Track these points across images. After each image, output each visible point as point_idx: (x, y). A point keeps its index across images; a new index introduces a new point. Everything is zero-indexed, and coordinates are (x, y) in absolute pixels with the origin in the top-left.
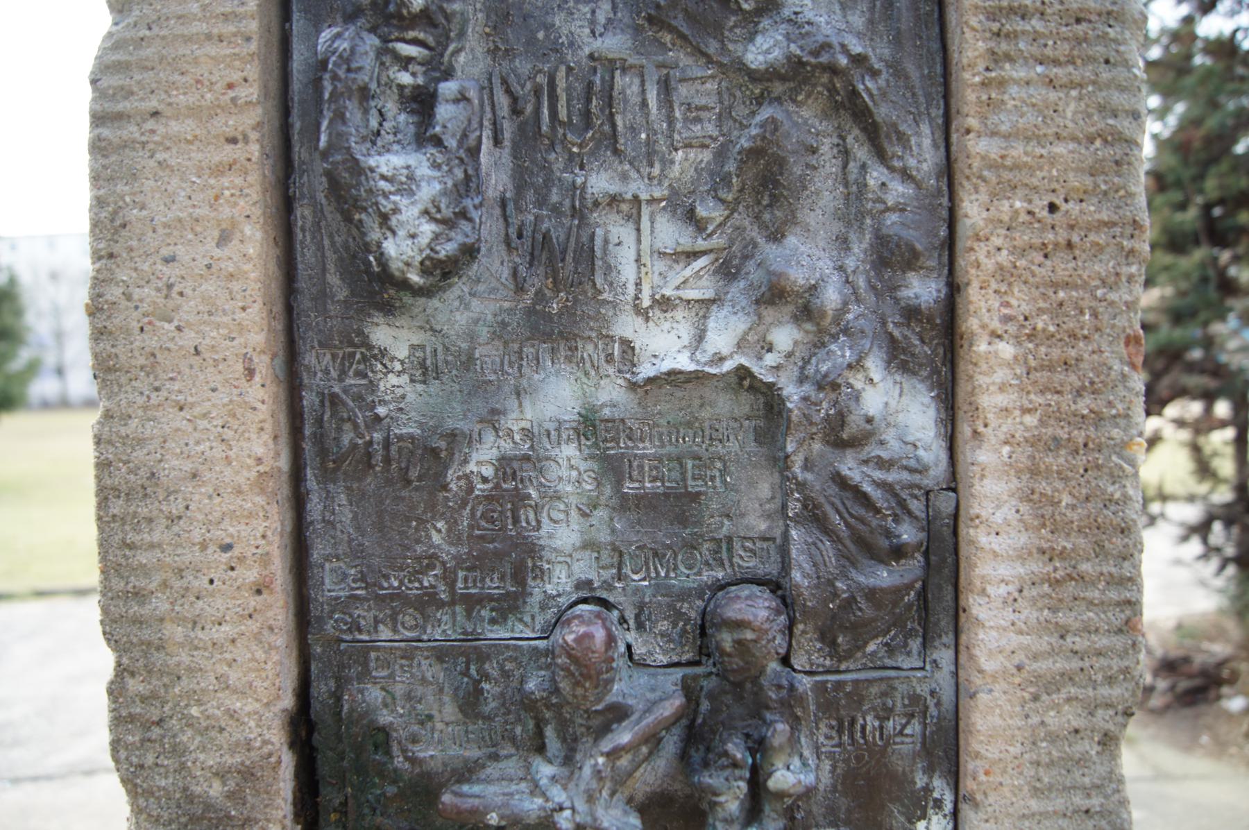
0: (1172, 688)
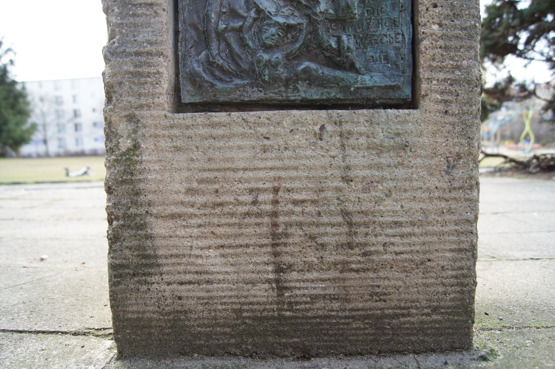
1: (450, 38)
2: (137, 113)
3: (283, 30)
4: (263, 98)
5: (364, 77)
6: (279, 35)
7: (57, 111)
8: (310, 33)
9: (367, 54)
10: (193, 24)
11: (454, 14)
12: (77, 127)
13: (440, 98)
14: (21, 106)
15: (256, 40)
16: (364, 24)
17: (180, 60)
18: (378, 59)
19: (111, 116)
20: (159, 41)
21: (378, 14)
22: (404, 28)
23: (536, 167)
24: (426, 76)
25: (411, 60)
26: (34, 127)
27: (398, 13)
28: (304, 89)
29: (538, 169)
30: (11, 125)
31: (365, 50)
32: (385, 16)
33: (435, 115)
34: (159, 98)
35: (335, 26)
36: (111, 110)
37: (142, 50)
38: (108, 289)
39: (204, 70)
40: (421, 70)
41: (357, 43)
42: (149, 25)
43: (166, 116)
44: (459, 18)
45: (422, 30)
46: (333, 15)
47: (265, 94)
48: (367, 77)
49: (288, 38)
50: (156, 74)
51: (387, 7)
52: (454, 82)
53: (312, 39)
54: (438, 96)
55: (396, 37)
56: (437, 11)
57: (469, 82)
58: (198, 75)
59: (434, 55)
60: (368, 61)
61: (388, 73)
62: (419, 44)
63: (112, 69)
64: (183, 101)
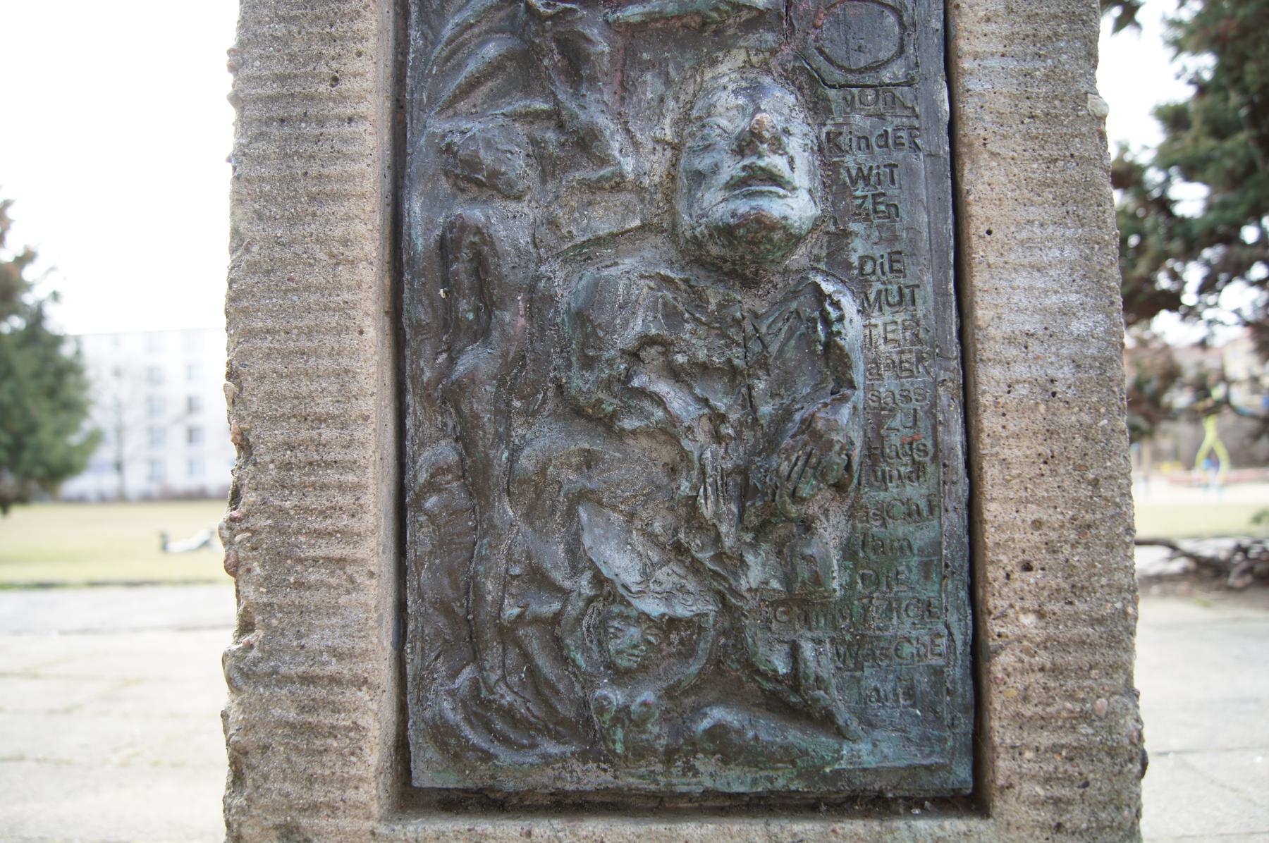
1: (1064, 647)
2: (304, 822)
3: (660, 629)
4: (610, 786)
5: (857, 747)
6: (649, 642)
7: (150, 399)
8: (725, 633)
9: (863, 683)
10: (442, 602)
11: (1073, 586)
12: (192, 435)
13: (1042, 793)
14: (70, 392)
15: (594, 647)
16: (855, 610)
17: (409, 685)
18: (891, 696)
19: (240, 825)
20: (357, 651)
21: (888, 586)
22: (953, 618)
23: (1245, 572)
24: (1008, 741)
25: (969, 695)
26: (95, 438)
27: (936, 587)
28: (711, 769)
29: (1248, 579)
30: (45, 435)
31: (858, 674)
32: (905, 593)
33: (1031, 835)
34: (357, 788)
35: (784, 613)
36: (243, 811)
37: (317, 670)
39: (467, 720)
40: (995, 724)
41: (838, 654)
42: (333, 610)
43: (373, 833)
44: (1085, 594)
45: (997, 629)
46: (779, 592)
47: (616, 777)
48: (864, 747)
49: (670, 644)
50: (351, 730)
51: (910, 571)
52: (1075, 754)
53: (730, 650)
54: (1038, 789)
55: (932, 642)
56: (1032, 581)
57: (1112, 752)
58: (453, 731)
59: (1026, 689)
60: (864, 700)
61: (914, 733)
62: (989, 660)
63: (244, 712)
64: (416, 784)
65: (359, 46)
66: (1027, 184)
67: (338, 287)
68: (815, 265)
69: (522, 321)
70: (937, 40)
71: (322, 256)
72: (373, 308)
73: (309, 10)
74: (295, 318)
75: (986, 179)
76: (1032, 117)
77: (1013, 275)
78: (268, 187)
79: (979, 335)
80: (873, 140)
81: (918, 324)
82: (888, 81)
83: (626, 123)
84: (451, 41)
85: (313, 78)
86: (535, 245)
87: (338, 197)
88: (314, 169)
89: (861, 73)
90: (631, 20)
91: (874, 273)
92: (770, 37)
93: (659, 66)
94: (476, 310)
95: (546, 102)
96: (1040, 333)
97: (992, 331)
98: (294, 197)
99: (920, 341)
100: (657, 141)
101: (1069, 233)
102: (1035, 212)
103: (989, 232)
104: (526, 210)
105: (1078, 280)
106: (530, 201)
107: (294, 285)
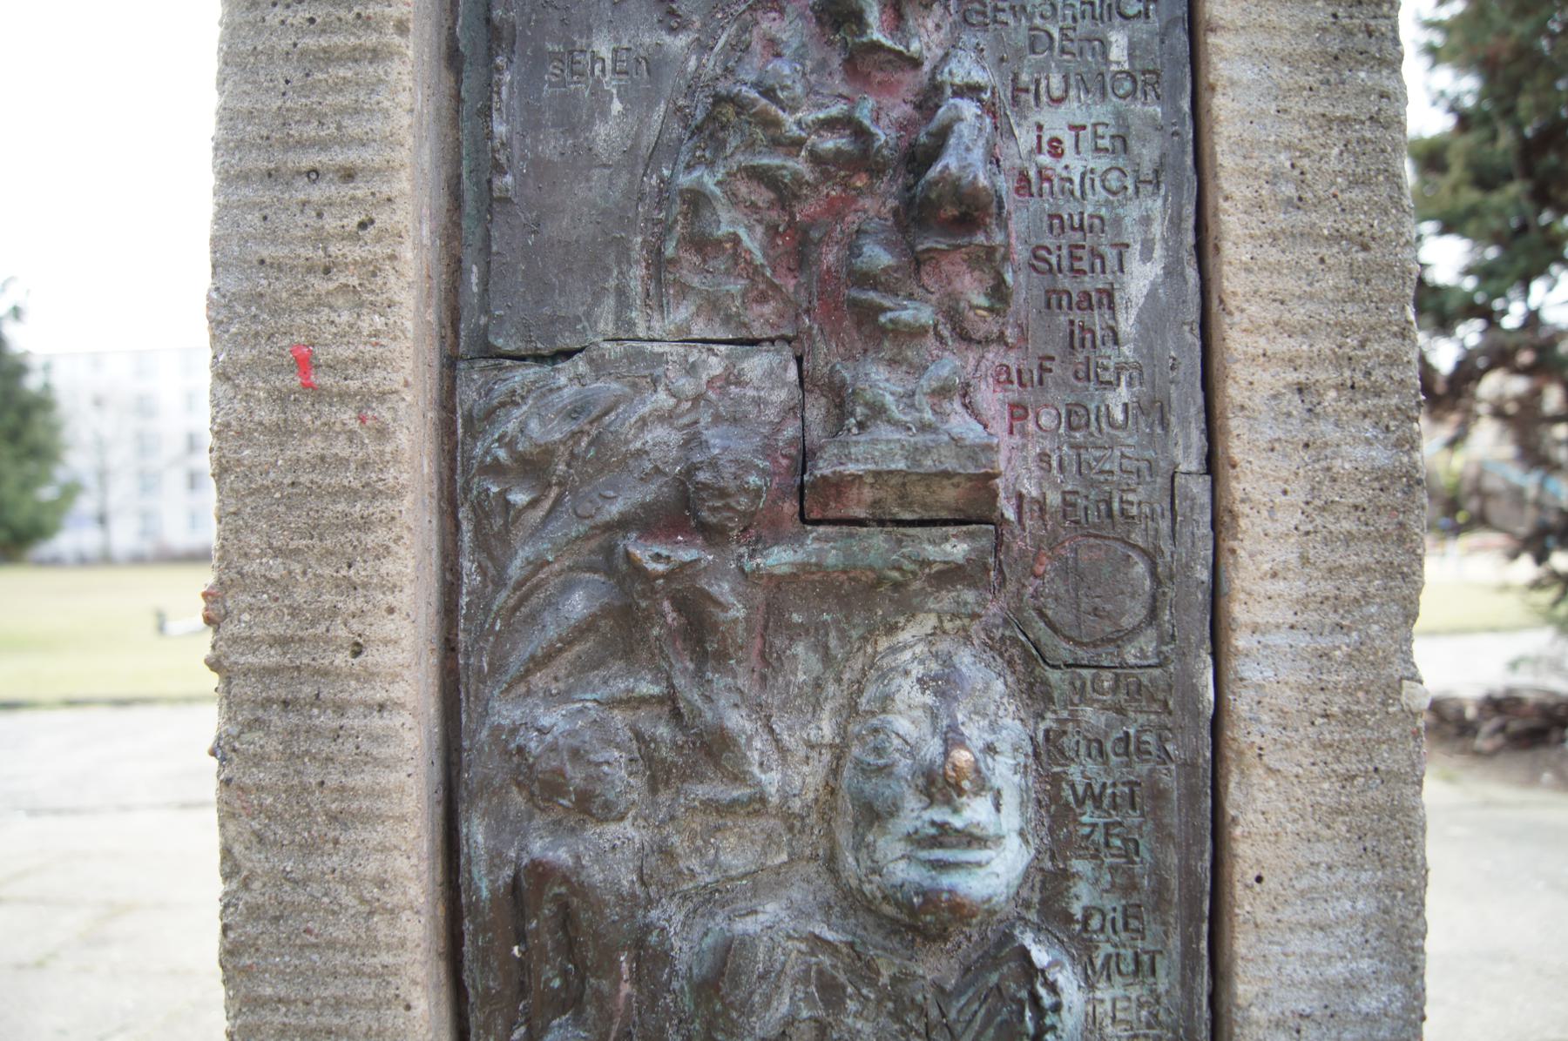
0: (1502, 729)
14: (38, 433)
26: (71, 491)
38: (220, 993)
65: (390, 598)
66: (1314, 813)
67: (373, 945)
68: (1024, 913)
69: (626, 988)
70: (1201, 597)
71: (348, 900)
72: (422, 974)
73: (315, 541)
74: (316, 983)
75: (1259, 805)
76: (1326, 716)
77: (1288, 936)
78: (270, 800)
79: (1238, 1016)
80: (1108, 746)
81: (1158, 1001)
82: (1132, 661)
83: (769, 717)
84: (520, 584)
85: (326, 643)
86: (643, 883)
87: (370, 818)
88: (333, 779)
89: (1095, 646)
90: (777, 571)
91: (1102, 929)
92: (970, 596)
93: (815, 632)
94: (564, 974)
95: (655, 682)
96: (1318, 1013)
97: (1255, 1012)
98: (308, 815)
99: (1159, 1023)
100: (811, 746)
101: (1365, 877)
102: (1323, 853)
103: (1259, 879)
104: (631, 832)
105: (1372, 940)
106: (635, 819)
107: (313, 940)
